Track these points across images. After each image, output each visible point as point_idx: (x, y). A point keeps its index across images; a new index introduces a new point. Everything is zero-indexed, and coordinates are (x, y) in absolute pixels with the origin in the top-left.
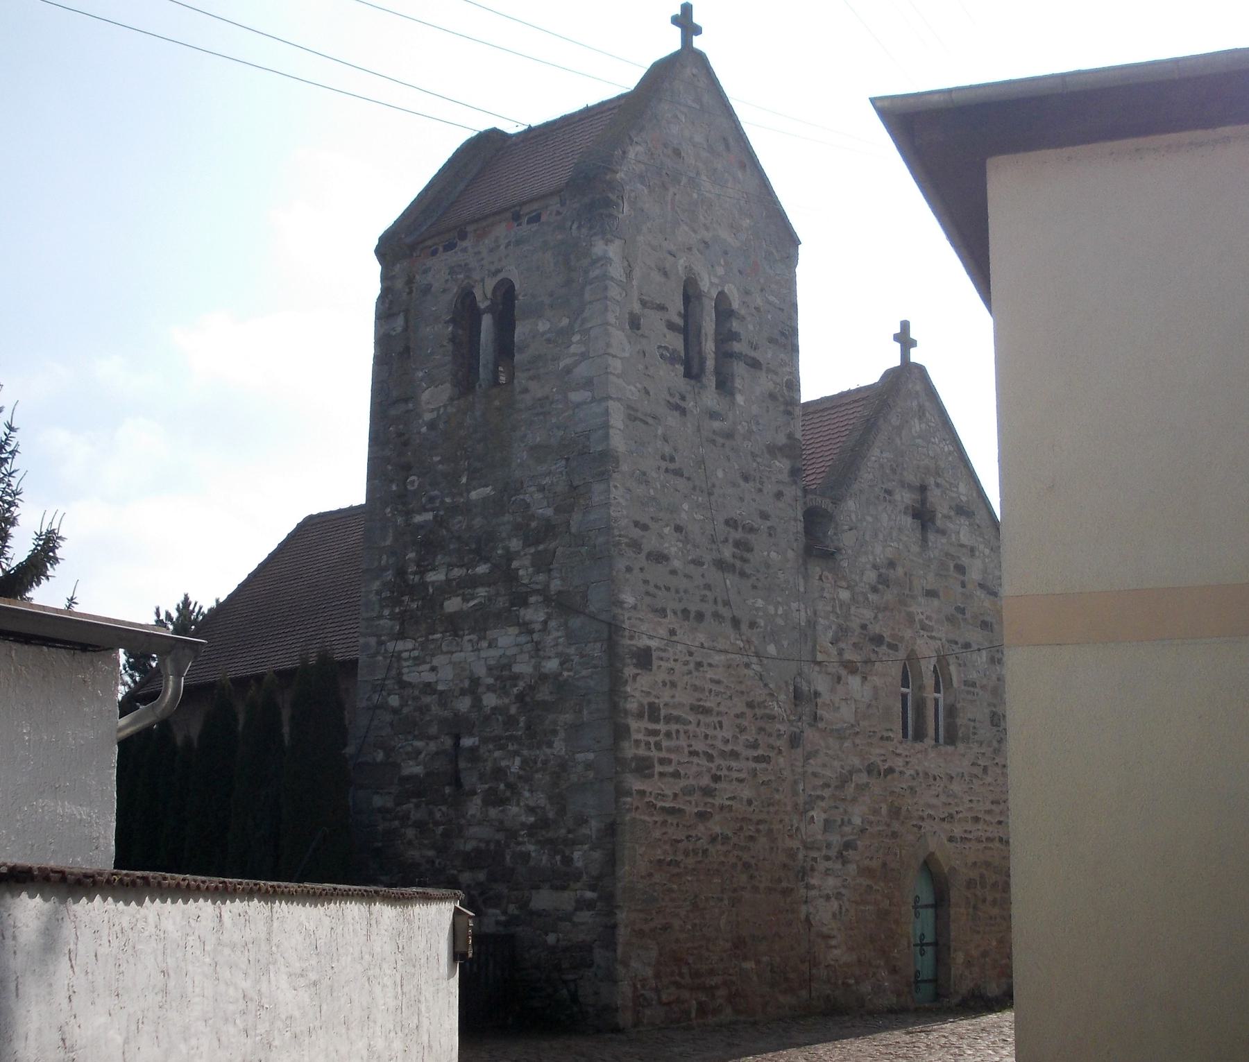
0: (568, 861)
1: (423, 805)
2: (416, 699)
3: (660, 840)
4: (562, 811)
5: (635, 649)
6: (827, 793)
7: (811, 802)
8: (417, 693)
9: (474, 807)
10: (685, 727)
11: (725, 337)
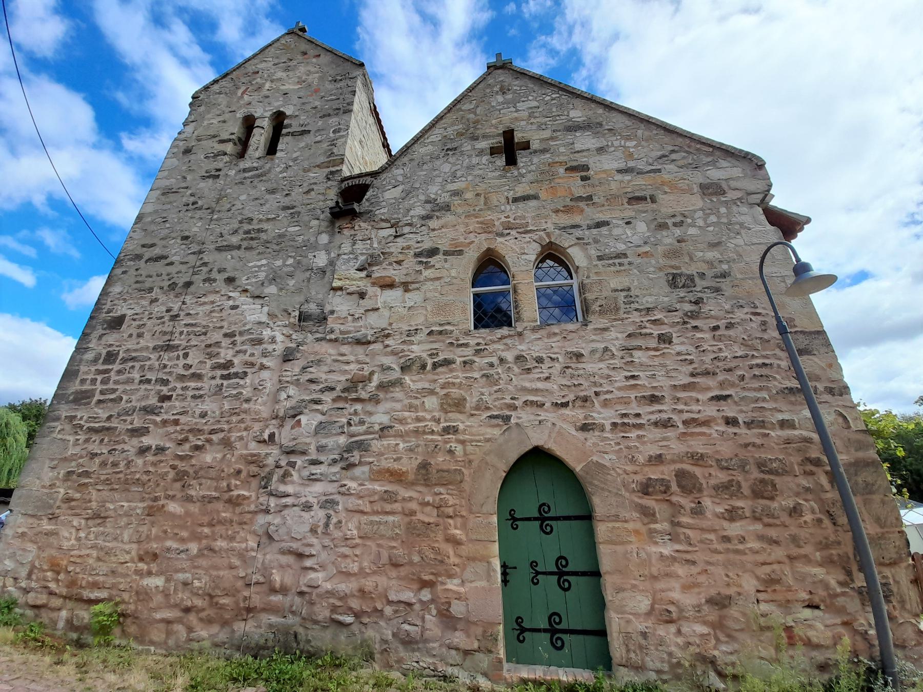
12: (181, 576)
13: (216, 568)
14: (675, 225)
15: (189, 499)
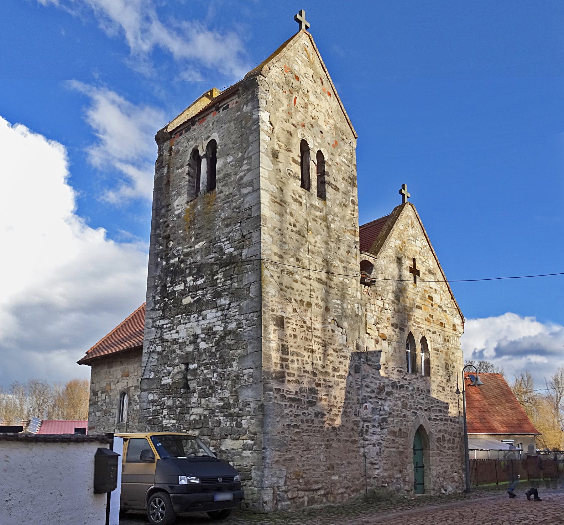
0: (239, 425)
1: (171, 398)
2: (169, 347)
3: (288, 414)
4: (237, 400)
5: (275, 317)
6: (373, 395)
7: (365, 400)
8: (169, 344)
9: (194, 399)
10: (302, 358)
11: (322, 173)
12: (344, 475)
13: (352, 470)
14: (149, 347)
15: (339, 440)
